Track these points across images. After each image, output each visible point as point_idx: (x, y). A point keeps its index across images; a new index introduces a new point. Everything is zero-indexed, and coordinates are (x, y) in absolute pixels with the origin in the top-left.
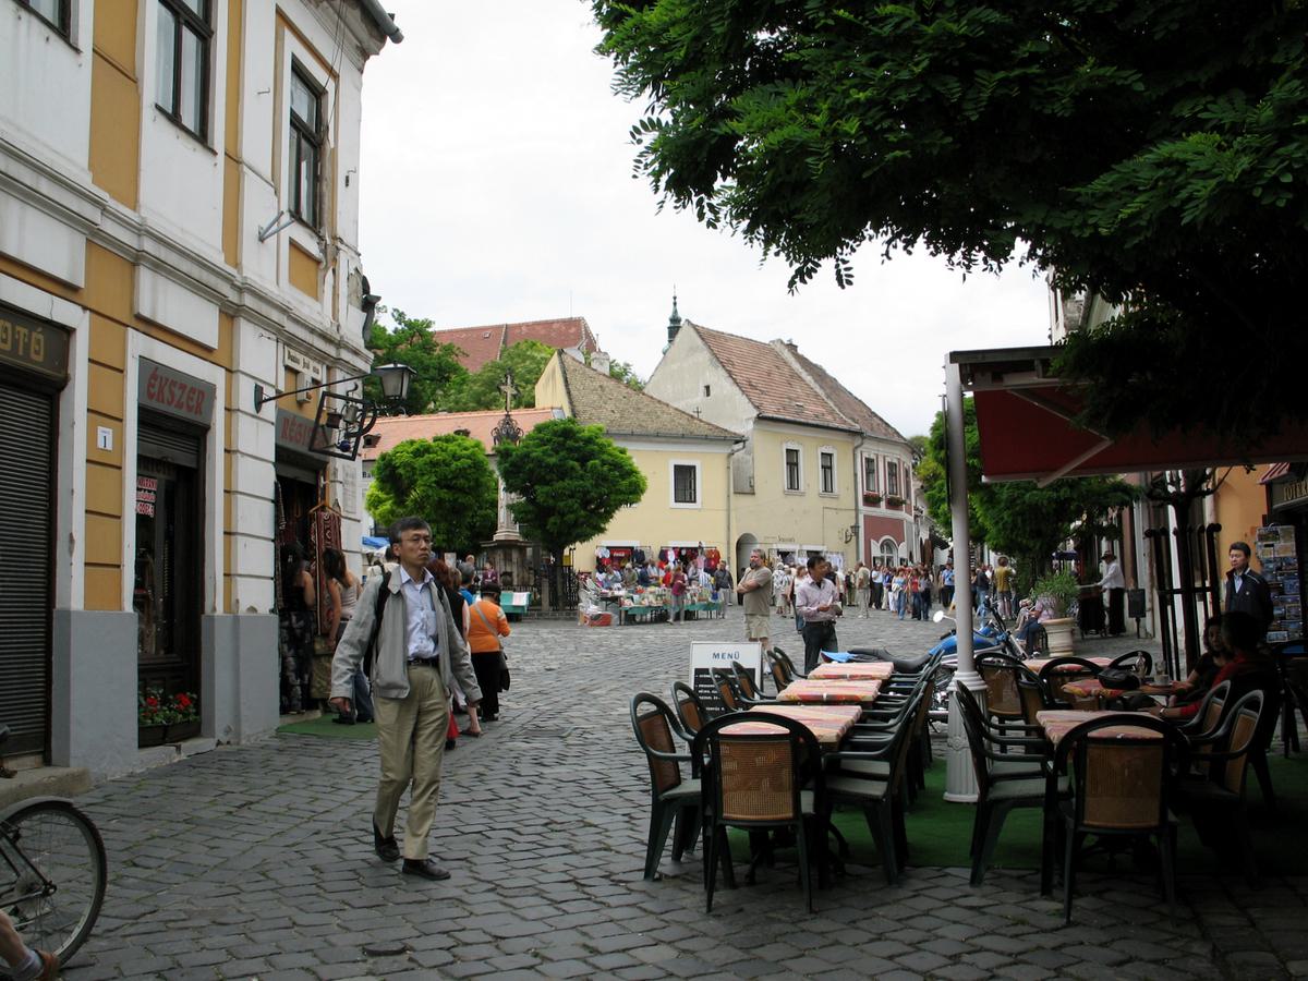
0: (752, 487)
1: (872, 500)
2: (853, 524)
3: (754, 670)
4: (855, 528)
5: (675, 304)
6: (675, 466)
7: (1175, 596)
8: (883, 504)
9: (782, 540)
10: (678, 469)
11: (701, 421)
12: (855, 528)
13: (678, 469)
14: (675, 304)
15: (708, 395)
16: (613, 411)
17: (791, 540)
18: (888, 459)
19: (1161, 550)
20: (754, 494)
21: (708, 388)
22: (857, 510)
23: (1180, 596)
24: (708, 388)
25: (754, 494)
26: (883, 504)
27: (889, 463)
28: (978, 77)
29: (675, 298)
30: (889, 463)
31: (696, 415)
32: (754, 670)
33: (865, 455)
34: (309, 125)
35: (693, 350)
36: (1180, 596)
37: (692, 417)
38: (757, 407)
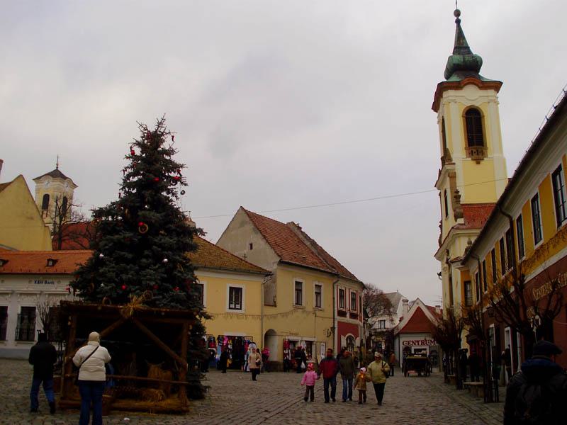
0: (275, 302)
1: (342, 314)
4: (333, 329)
5: (458, 22)
6: (7, 307)
8: (348, 315)
9: (291, 334)
10: (231, 289)
11: (246, 262)
12: (333, 329)
13: (231, 289)
14: (458, 22)
15: (251, 248)
17: (296, 335)
18: (351, 291)
21: (251, 245)
22: (334, 318)
24: (251, 245)
26: (348, 315)
27: (340, 290)
30: (340, 290)
31: (243, 258)
33: (339, 287)
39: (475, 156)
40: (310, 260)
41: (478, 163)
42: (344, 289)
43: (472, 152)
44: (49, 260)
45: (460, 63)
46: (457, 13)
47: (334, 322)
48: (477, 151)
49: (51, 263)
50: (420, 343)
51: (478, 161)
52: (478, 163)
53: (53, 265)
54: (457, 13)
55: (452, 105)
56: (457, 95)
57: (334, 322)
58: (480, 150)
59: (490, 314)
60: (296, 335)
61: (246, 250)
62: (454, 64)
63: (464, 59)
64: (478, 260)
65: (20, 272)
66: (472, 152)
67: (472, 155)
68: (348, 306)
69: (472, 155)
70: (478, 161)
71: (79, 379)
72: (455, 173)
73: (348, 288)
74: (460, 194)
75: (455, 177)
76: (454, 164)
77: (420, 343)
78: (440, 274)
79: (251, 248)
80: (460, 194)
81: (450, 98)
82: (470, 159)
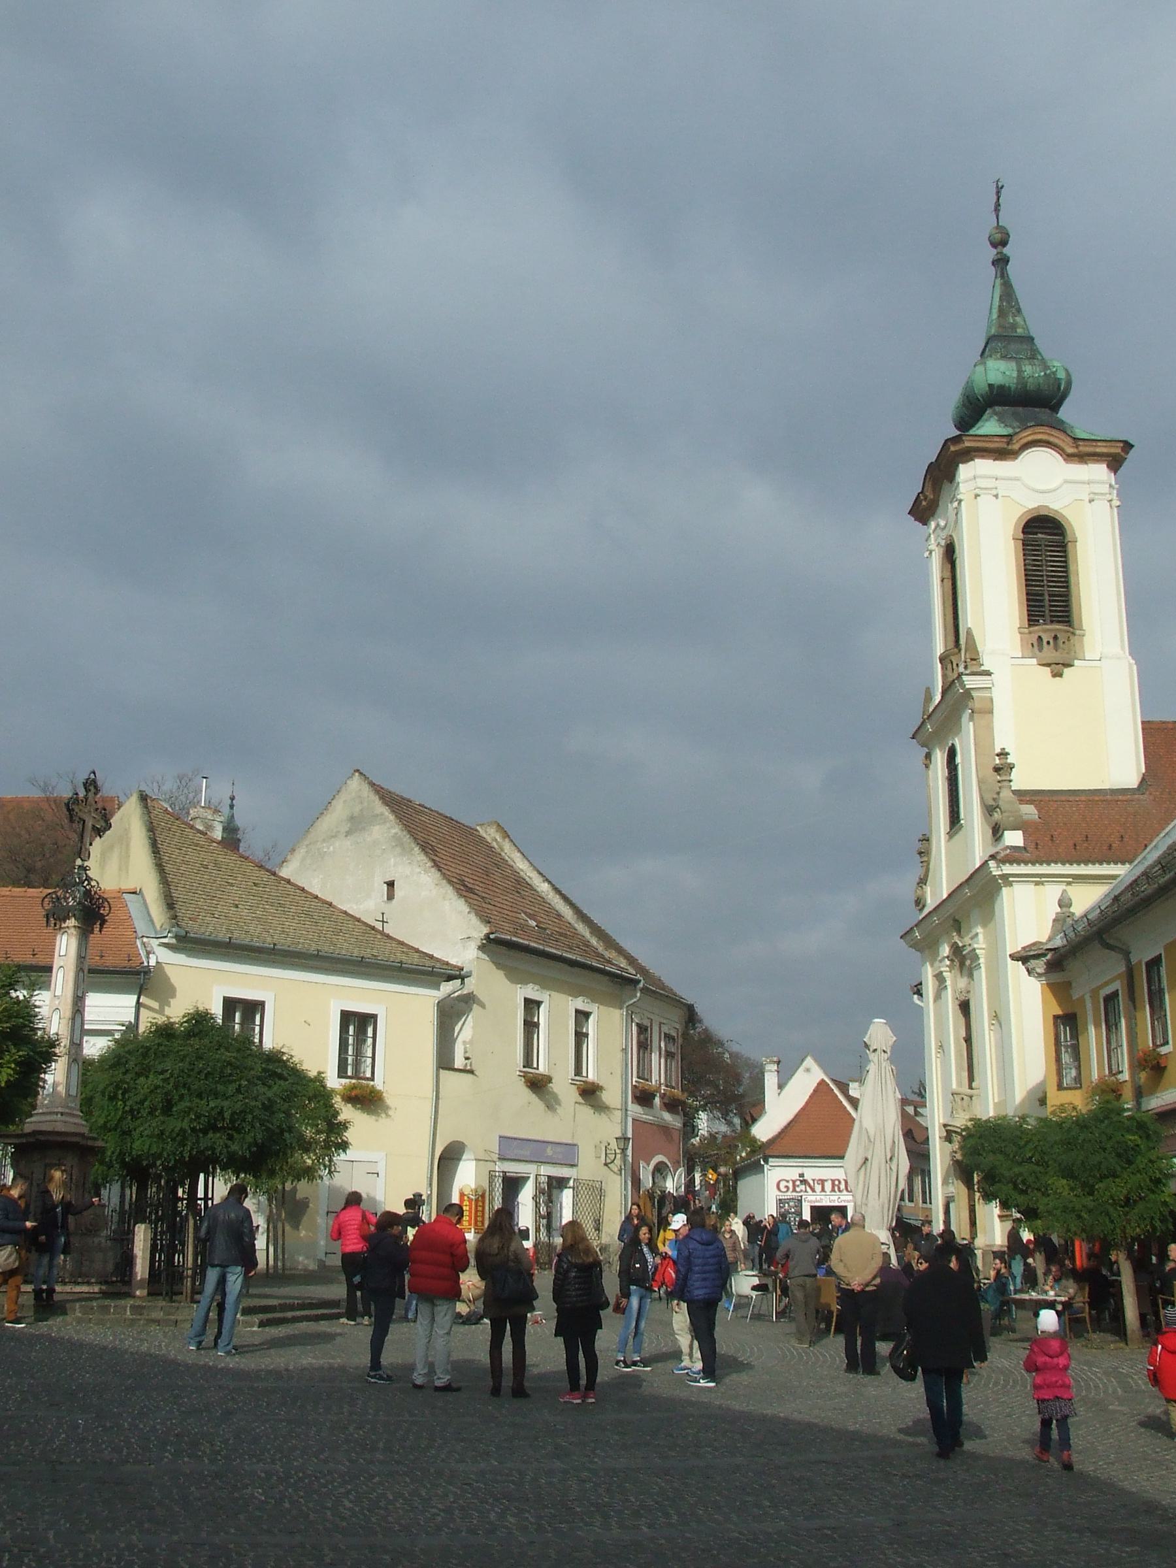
2: (619, 1135)
3: (823, 1080)
5: (1001, 262)
6: (342, 1011)
7: (203, 1196)
10: (347, 1017)
11: (388, 936)
13: (347, 1017)
14: (1001, 262)
15: (390, 897)
18: (665, 1029)
19: (208, 1186)
20: (500, 1137)
21: (391, 884)
23: (199, 1196)
24: (391, 884)
25: (500, 1137)
28: (678, 1334)
29: (232, 798)
31: (379, 926)
32: (823, 1080)
34: (1112, 886)
35: (357, 824)
36: (199, 1196)
37: (373, 928)
39: (1049, 653)
40: (346, 947)
42: (646, 1023)
45: (1009, 388)
46: (232, 798)
48: (1055, 638)
50: (828, 1186)
51: (1058, 668)
54: (1000, 241)
55: (985, 500)
56: (1000, 474)
62: (990, 386)
63: (1020, 371)
64: (1126, 954)
67: (1041, 649)
69: (1041, 649)
70: (1058, 668)
71: (298, 1198)
72: (991, 700)
73: (657, 1019)
74: (1010, 760)
75: (991, 712)
76: (988, 673)
77: (828, 1186)
79: (390, 897)
80: (1010, 760)
81: (982, 483)
82: (1034, 661)
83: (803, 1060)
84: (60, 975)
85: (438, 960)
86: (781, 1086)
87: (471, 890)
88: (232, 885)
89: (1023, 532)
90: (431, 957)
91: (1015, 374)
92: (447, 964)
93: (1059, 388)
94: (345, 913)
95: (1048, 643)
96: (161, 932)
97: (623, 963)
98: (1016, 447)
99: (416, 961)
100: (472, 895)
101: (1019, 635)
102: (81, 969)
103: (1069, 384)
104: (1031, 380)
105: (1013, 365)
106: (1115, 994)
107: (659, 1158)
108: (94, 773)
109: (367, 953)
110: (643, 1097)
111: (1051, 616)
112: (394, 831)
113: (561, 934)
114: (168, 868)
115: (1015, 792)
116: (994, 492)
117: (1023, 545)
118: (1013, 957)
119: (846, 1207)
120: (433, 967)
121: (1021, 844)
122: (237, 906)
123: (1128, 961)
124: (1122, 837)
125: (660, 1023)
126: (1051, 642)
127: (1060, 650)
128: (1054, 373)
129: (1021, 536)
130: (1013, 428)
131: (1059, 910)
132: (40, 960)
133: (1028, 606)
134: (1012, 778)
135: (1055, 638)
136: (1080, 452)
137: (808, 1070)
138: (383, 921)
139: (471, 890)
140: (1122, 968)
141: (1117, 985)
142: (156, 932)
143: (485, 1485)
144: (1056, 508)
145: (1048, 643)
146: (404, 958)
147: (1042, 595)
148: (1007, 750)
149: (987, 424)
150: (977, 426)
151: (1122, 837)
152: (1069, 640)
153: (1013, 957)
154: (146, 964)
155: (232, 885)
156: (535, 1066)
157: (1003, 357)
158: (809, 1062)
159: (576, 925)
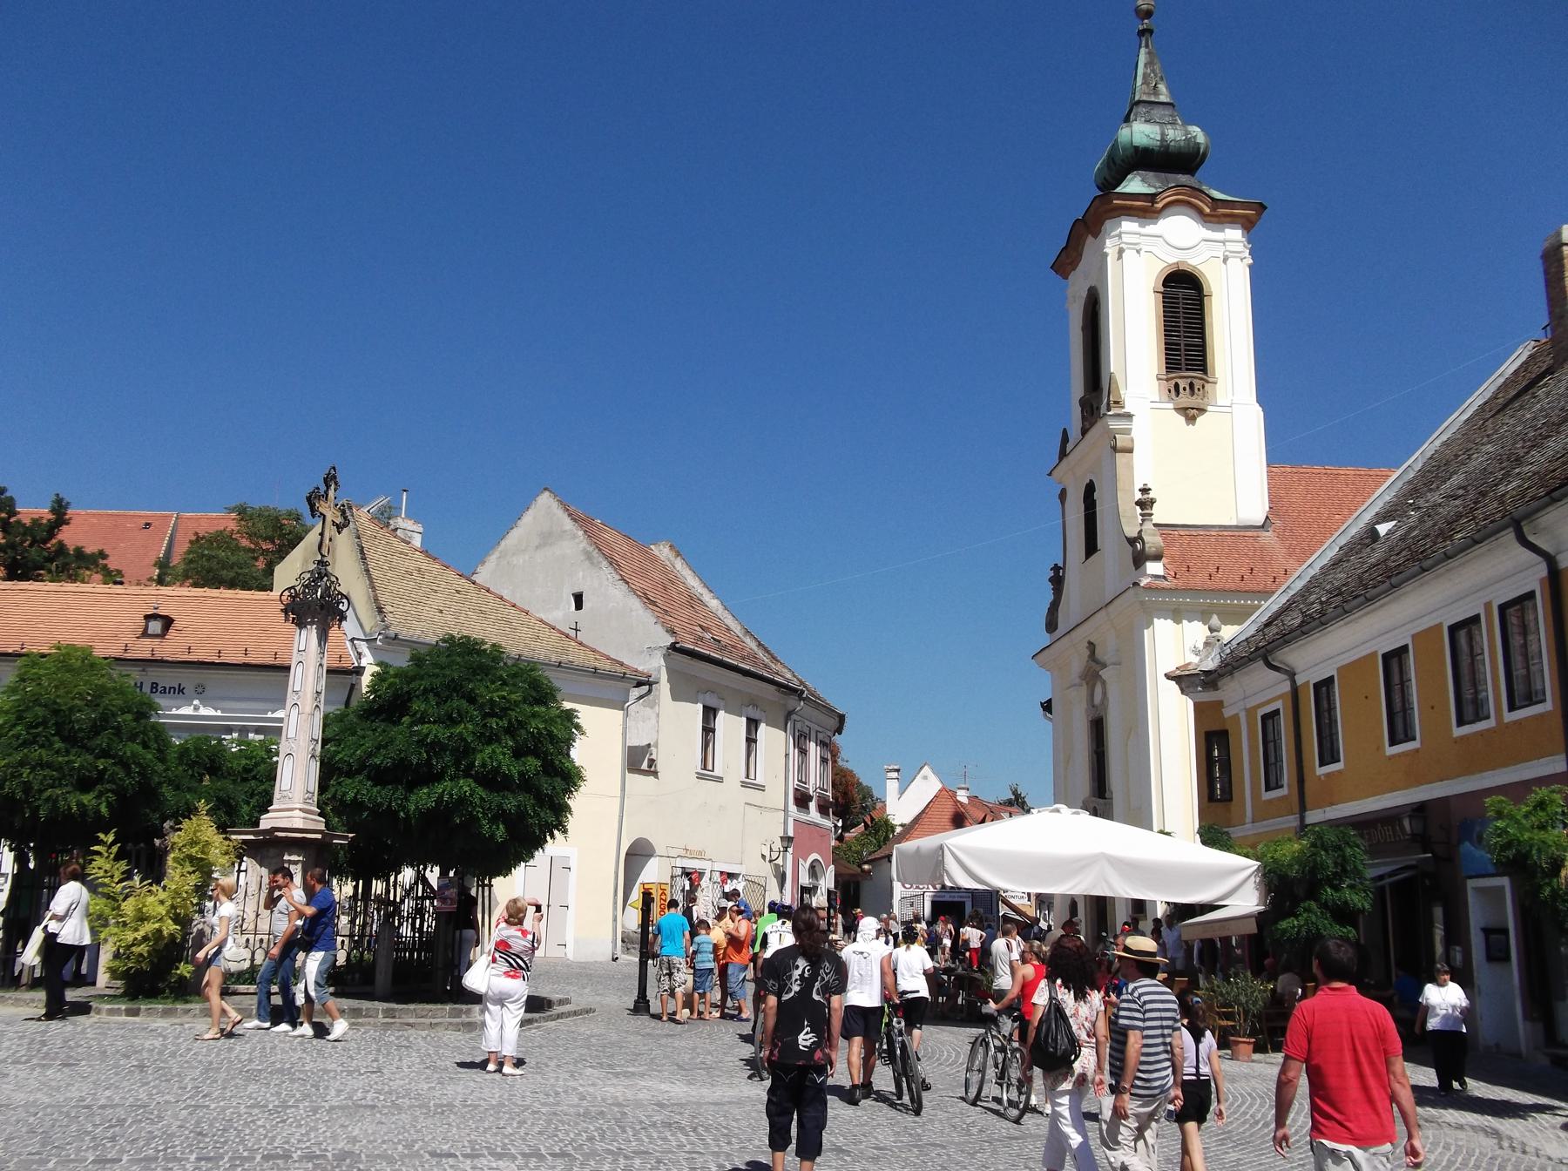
15: (579, 605)
16: (441, 612)
18: (821, 736)
22: (786, 810)
26: (813, 805)
31: (573, 634)
35: (547, 538)
38: (672, 632)
41: (1191, 420)
43: (1177, 386)
44: (148, 618)
47: (786, 823)
48: (1191, 386)
49: (155, 627)
51: (1191, 414)
52: (1191, 420)
53: (162, 635)
57: (786, 823)
58: (1197, 383)
59: (985, 951)
60: (700, 856)
61: (562, 613)
62: (1136, 148)
63: (1163, 134)
65: (241, 659)
66: (1177, 386)
68: (812, 781)
70: (1191, 414)
74: (1152, 495)
76: (1129, 416)
78: (1047, 707)
79: (579, 605)
80: (1152, 495)
82: (1171, 406)
83: (921, 768)
84: (300, 669)
85: (628, 667)
86: (902, 792)
87: (654, 603)
88: (436, 592)
89: (1164, 285)
90: (622, 664)
91: (1159, 138)
92: (636, 671)
93: (1199, 149)
94: (541, 621)
95: (1185, 389)
96: (371, 634)
97: (789, 676)
98: (1160, 205)
99: (608, 667)
100: (655, 608)
101: (1156, 383)
102: (321, 665)
103: (1205, 155)
104: (1172, 144)
105: (1157, 129)
106: (1277, 712)
107: (814, 856)
108: (334, 468)
109: (564, 658)
110: (802, 800)
111: (1187, 365)
112: (582, 546)
113: (733, 647)
114: (375, 573)
115: (1155, 525)
116: (1138, 247)
117: (1164, 297)
118: (1168, 676)
119: (964, 902)
120: (625, 674)
121: (1162, 574)
122: (441, 612)
123: (1293, 682)
124: (1252, 569)
125: (817, 731)
126: (1188, 388)
127: (1195, 396)
128: (1195, 137)
129: (1162, 289)
130: (1156, 188)
131: (1209, 633)
132: (1130, 446)
133: (1166, 354)
134: (1153, 512)
135: (1191, 386)
136: (1215, 215)
137: (925, 778)
138: (576, 630)
139: (654, 603)
140: (1286, 687)
141: (1278, 705)
142: (365, 635)
143: (6, 780)
144: (1194, 264)
145: (1185, 389)
146: (597, 664)
147: (1179, 345)
148: (1149, 486)
149: (1132, 183)
150: (1122, 185)
151: (1252, 569)
152: (1203, 387)
153: (1168, 676)
154: (356, 665)
155: (436, 592)
156: (711, 768)
157: (1147, 121)
158: (926, 770)
159: (744, 639)
